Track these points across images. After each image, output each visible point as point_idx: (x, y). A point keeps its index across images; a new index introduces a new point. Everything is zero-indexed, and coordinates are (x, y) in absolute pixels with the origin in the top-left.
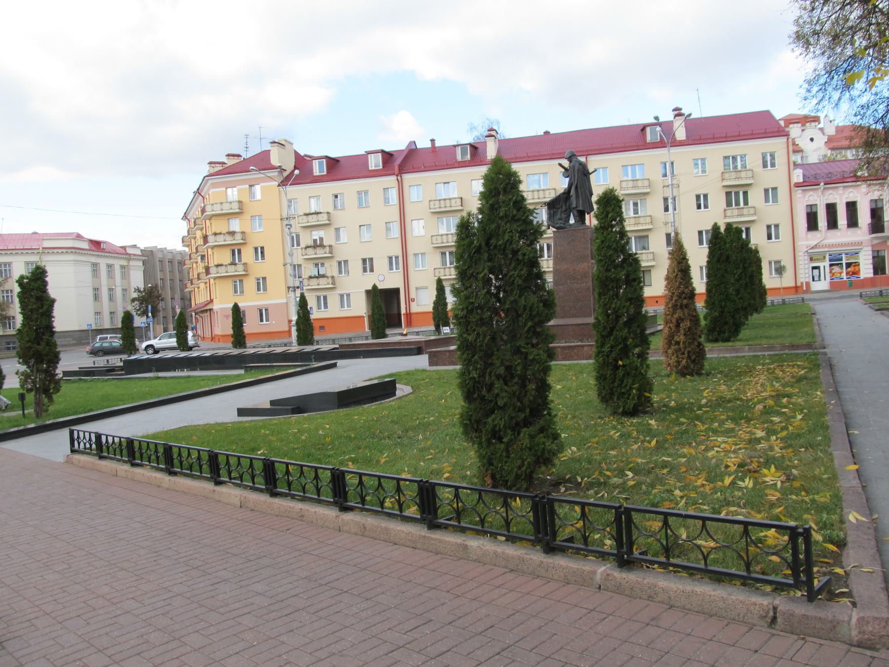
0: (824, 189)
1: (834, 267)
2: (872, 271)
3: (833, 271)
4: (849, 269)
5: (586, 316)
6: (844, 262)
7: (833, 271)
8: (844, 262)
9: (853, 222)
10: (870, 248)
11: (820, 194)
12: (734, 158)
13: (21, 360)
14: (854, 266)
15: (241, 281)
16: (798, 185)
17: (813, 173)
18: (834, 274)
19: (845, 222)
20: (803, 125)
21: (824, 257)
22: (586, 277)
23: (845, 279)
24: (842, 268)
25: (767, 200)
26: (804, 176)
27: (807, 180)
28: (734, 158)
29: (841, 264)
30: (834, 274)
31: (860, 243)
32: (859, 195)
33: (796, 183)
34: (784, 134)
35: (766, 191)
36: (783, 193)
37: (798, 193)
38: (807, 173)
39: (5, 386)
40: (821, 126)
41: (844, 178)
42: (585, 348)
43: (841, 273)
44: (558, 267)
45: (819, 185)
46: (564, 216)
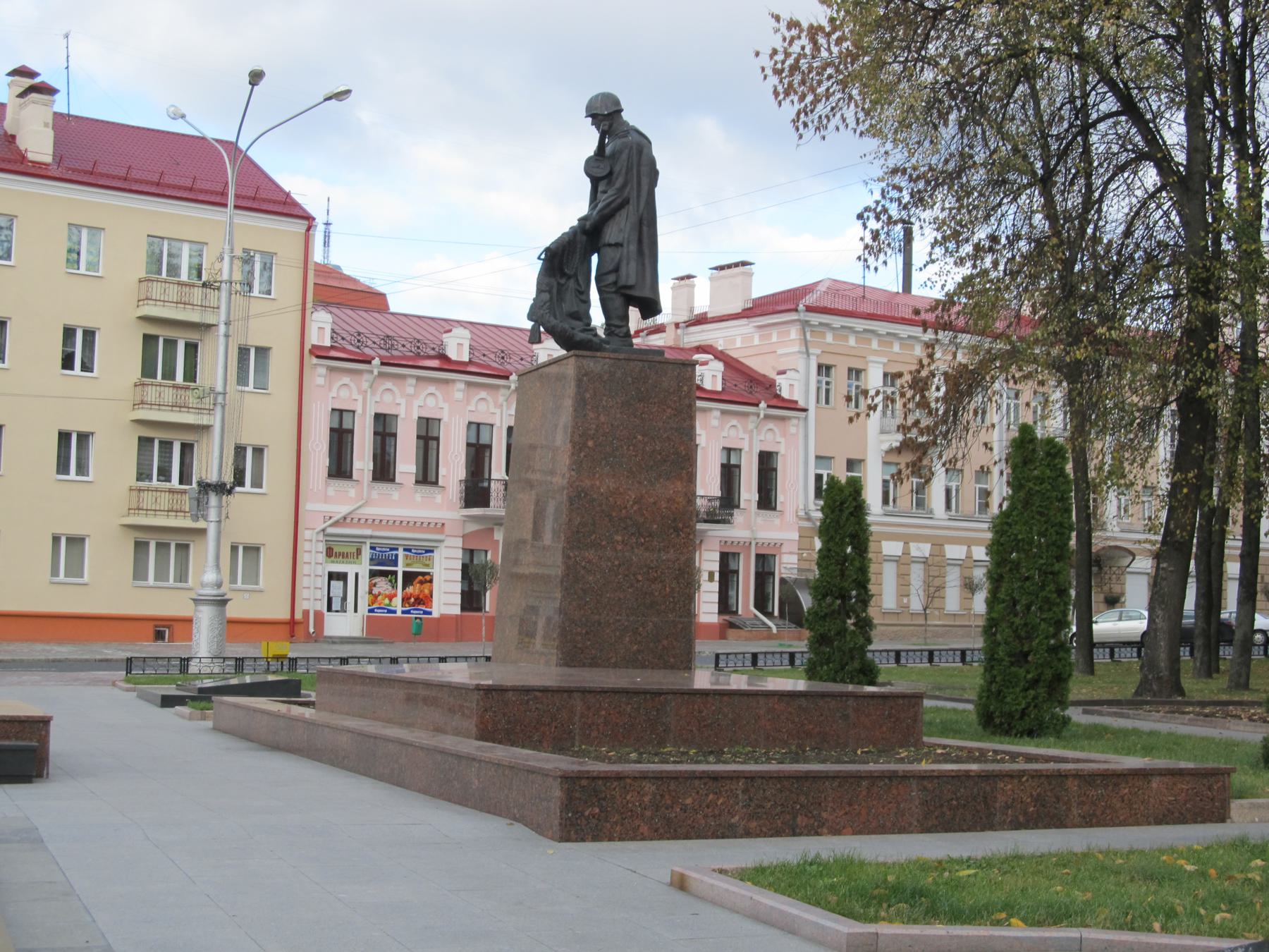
1: (377, 580)
2: (458, 599)
3: (376, 591)
4: (410, 590)
5: (672, 667)
6: (400, 569)
7: (376, 591)
8: (400, 569)
9: (427, 476)
10: (459, 542)
11: (365, 385)
14: (421, 583)
15: (182, 548)
16: (320, 353)
18: (376, 597)
21: (359, 552)
22: (676, 530)
23: (399, 614)
24: (394, 586)
29: (395, 573)
30: (376, 597)
31: (440, 527)
32: (446, 406)
33: (314, 347)
36: (282, 364)
37: (318, 373)
39: (631, 308)
41: (418, 356)
43: (391, 597)
44: (587, 483)
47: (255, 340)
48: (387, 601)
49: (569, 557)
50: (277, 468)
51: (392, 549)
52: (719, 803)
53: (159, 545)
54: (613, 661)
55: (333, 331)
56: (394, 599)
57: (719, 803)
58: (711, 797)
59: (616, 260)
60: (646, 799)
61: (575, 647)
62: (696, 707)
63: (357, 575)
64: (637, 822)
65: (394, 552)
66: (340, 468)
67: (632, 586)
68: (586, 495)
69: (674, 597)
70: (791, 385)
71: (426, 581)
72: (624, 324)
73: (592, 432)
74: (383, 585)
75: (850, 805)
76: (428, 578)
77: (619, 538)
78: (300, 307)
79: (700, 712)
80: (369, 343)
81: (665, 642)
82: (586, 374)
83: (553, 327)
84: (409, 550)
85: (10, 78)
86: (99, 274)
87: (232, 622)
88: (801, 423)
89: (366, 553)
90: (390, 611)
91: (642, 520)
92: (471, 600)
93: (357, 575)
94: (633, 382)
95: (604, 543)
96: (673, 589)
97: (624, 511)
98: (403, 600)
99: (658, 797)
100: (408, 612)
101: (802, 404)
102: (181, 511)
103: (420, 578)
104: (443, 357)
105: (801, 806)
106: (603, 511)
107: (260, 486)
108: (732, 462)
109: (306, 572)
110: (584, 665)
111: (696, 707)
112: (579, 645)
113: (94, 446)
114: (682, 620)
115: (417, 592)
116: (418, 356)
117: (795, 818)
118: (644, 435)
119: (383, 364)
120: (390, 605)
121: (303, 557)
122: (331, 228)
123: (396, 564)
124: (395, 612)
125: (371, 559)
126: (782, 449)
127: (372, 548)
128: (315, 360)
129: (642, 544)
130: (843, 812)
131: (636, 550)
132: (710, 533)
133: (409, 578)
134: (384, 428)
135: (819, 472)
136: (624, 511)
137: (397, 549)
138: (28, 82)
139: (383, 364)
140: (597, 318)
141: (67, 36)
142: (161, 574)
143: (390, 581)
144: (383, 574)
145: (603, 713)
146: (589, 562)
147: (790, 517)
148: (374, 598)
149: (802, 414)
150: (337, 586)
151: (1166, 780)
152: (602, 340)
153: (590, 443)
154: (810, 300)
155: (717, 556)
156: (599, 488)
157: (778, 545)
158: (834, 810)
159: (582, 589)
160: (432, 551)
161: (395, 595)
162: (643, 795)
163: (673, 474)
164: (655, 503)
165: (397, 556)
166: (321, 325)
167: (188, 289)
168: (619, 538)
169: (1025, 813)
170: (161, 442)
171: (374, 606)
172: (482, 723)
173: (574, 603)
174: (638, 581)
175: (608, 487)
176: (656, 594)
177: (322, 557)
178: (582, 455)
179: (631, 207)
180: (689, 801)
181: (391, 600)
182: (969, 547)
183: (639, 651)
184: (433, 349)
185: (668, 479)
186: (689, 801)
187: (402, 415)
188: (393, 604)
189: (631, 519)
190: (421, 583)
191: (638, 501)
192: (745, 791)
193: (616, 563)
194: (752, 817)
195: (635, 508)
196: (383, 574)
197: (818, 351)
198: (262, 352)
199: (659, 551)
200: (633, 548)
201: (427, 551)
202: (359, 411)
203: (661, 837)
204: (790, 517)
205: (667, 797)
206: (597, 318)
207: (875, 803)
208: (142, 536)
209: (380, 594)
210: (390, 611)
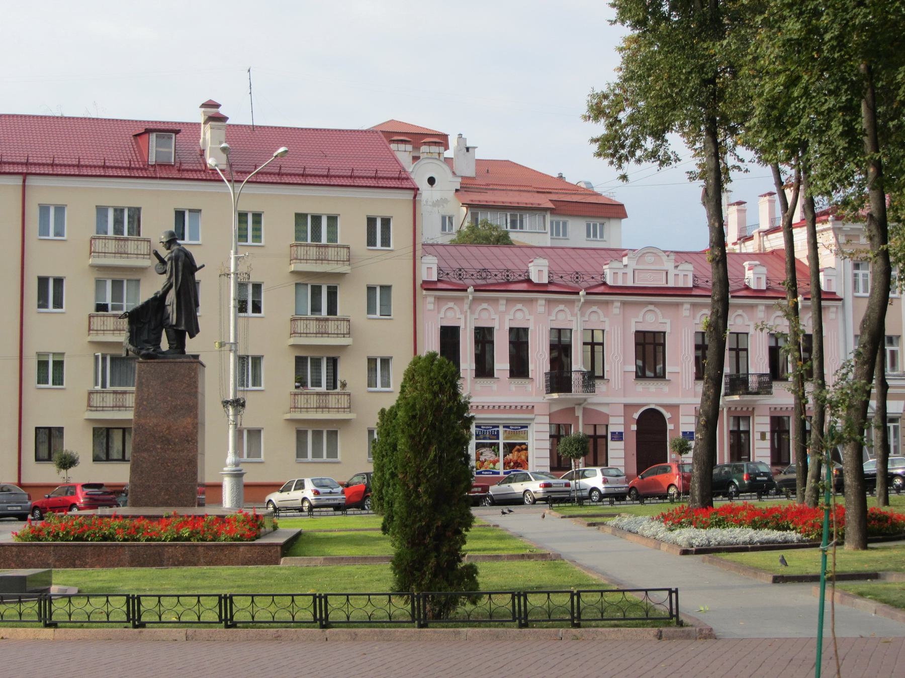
0: (474, 299)
1: (483, 450)
2: (547, 462)
3: (482, 458)
4: (510, 457)
5: (186, 506)
6: (501, 441)
7: (482, 458)
8: (501, 441)
9: (519, 368)
10: (546, 419)
11: (466, 307)
12: (317, 219)
14: (519, 451)
15: (333, 434)
16: (428, 286)
17: (456, 266)
18: (483, 463)
19: (507, 366)
20: (416, 148)
22: (188, 441)
23: (502, 474)
25: (371, 309)
26: (440, 269)
27: (445, 278)
28: (317, 219)
29: (498, 444)
30: (483, 463)
31: (530, 409)
32: (531, 318)
33: (425, 282)
34: (406, 184)
35: (371, 289)
36: (401, 299)
37: (428, 301)
38: (443, 265)
40: (448, 154)
41: (509, 282)
42: (241, 549)
43: (495, 463)
44: (143, 421)
45: (466, 290)
46: (153, 337)
47: (377, 281)
48: (491, 466)
49: (134, 456)
51: (522, 427)
53: (314, 432)
56: (497, 464)
60: (14, 554)
64: (10, 562)
65: (496, 429)
67: (165, 468)
70: (829, 280)
71: (522, 450)
76: (524, 447)
77: (159, 446)
78: (412, 254)
81: (182, 494)
84: (508, 427)
85: (203, 109)
86: (263, 243)
87: (247, 486)
88: (840, 310)
90: (494, 473)
92: (779, 456)
96: (186, 470)
98: (504, 464)
101: (840, 294)
102: (326, 408)
104: (528, 281)
107: (388, 385)
108: (779, 345)
113: (264, 364)
115: (515, 458)
116: (509, 282)
117: (74, 561)
118: (171, 397)
119: (476, 291)
120: (494, 468)
123: (498, 438)
124: (498, 473)
127: (477, 427)
128: (424, 292)
132: (759, 403)
133: (510, 447)
134: (484, 337)
137: (498, 427)
138: (212, 111)
139: (476, 291)
141: (249, 71)
142: (317, 453)
143: (494, 450)
146: (144, 458)
149: (839, 303)
151: (247, 548)
155: (767, 420)
160: (527, 427)
161: (498, 461)
165: (498, 431)
166: (429, 266)
167: (323, 249)
169: (178, 561)
170: (311, 359)
171: (482, 470)
180: (31, 554)
181: (494, 465)
184: (520, 275)
186: (31, 554)
187: (497, 327)
188: (496, 467)
190: (519, 451)
191: (169, 428)
192: (53, 551)
194: (57, 561)
198: (386, 289)
201: (522, 427)
203: (20, 568)
208: (302, 427)
209: (485, 460)
210: (494, 473)
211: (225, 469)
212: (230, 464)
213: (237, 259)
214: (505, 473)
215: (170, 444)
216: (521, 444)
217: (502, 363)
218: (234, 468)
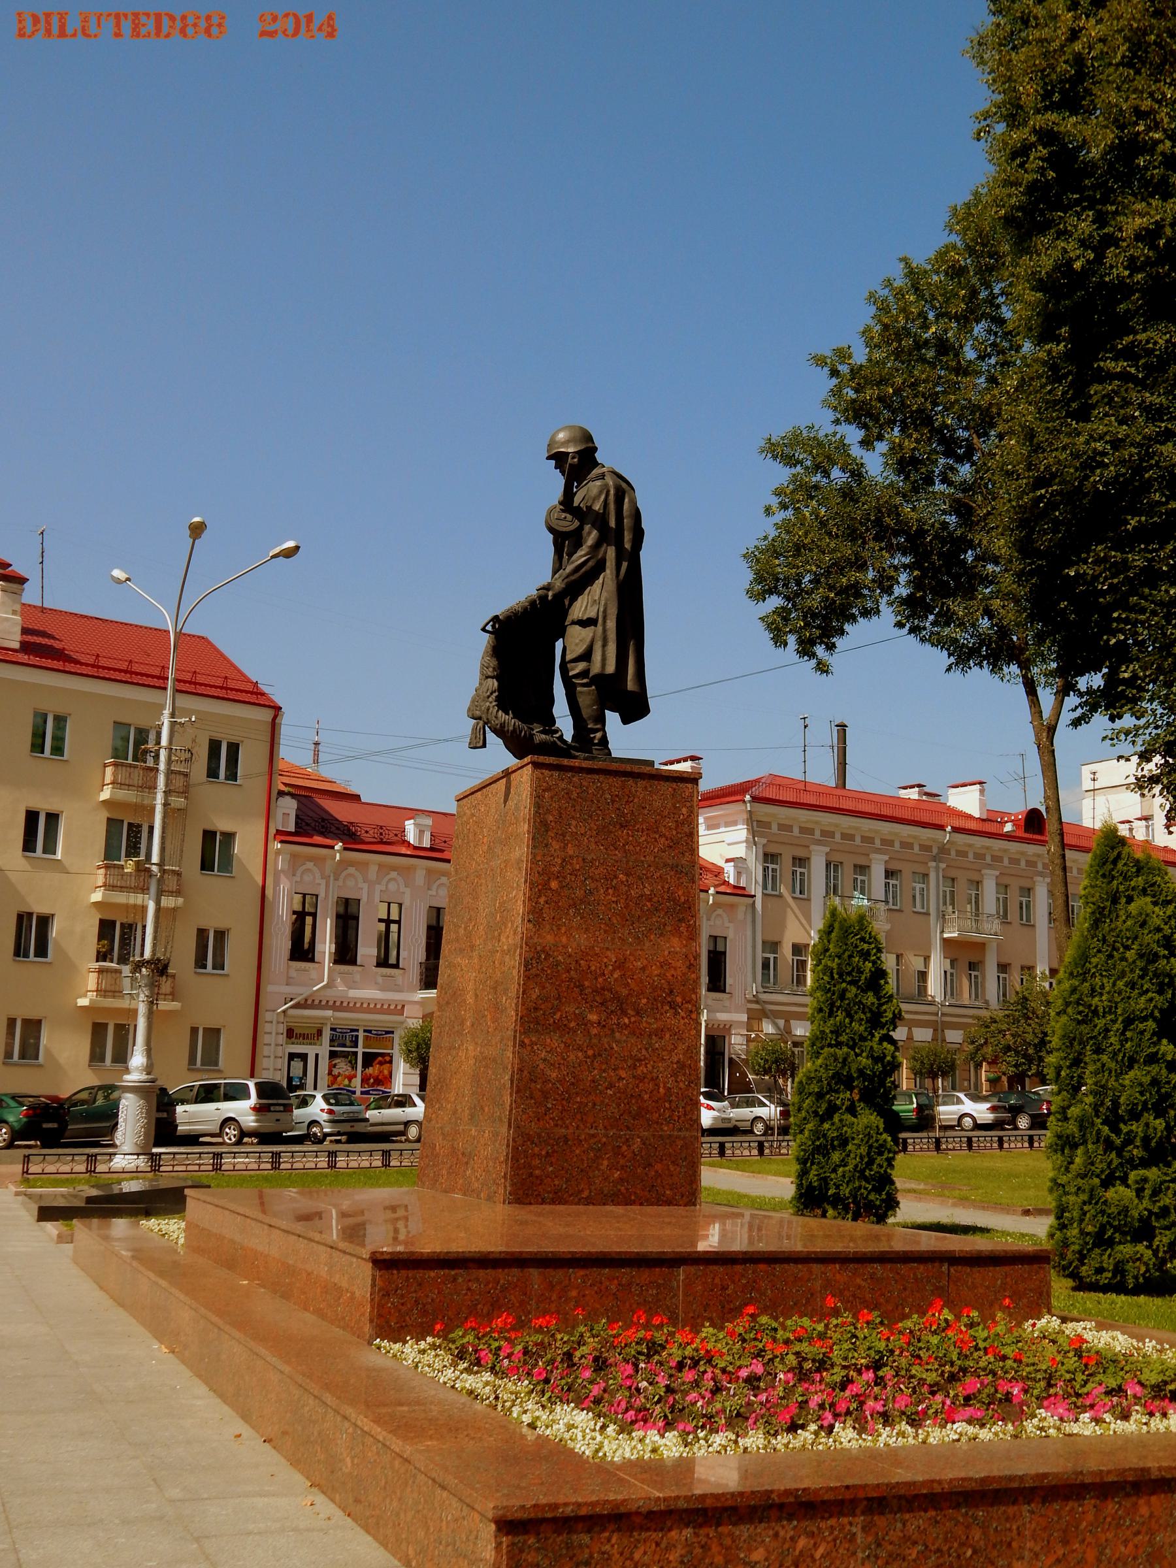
1: (337, 1061)
3: (335, 1072)
4: (370, 1070)
5: (669, 1203)
6: (360, 1050)
7: (335, 1072)
8: (360, 1050)
13: (882, 982)
14: (381, 1063)
18: (335, 1077)
21: (320, 1033)
22: (673, 1006)
23: (358, 1094)
24: (354, 1067)
29: (355, 1054)
32: (408, 891)
39: (607, 712)
43: (350, 1078)
44: (550, 938)
48: (346, 1082)
50: (239, 952)
51: (387, 1032)
52: (818, 1555)
54: (585, 1194)
55: (297, 816)
57: (818, 1555)
58: (802, 1542)
59: (588, 640)
61: (531, 1175)
62: (717, 1281)
63: (317, 1055)
66: (302, 951)
68: (548, 955)
69: (670, 1102)
71: (386, 1062)
72: (599, 726)
73: (557, 869)
74: (342, 1067)
75: (1065, 1542)
76: (387, 1058)
77: (593, 1017)
79: (724, 1288)
80: (333, 829)
81: (658, 1167)
82: (548, 789)
83: (503, 725)
86: (65, 758)
89: (327, 1034)
91: (625, 992)
93: (317, 1055)
94: (613, 801)
95: (572, 1024)
97: (600, 980)
99: (698, 1551)
100: (367, 1093)
103: (380, 1058)
105: (975, 1552)
106: (571, 979)
109: (266, 1053)
110: (543, 1202)
111: (717, 1281)
112: (537, 1172)
114: (682, 1134)
118: (627, 875)
121: (264, 1039)
122: (320, 747)
124: (354, 1092)
125: (332, 1040)
126: (730, 935)
127: (332, 1029)
129: (627, 1026)
130: (1052, 1559)
131: (617, 1035)
135: (768, 955)
136: (600, 980)
137: (357, 1030)
140: (565, 725)
143: (350, 1062)
144: (345, 1055)
145: (574, 1293)
147: (738, 998)
148: (334, 1078)
150: (297, 1065)
152: (569, 746)
153: (554, 885)
154: (755, 791)
156: (565, 947)
157: (727, 1028)
158: (1037, 1555)
159: (541, 1090)
160: (392, 1032)
161: (355, 1076)
162: (668, 1549)
163: (669, 928)
164: (643, 969)
165: (357, 1037)
166: (286, 811)
168: (593, 1017)
172: (380, 1316)
173: (529, 1111)
174: (621, 1079)
175: (579, 945)
176: (646, 1097)
177: (282, 1039)
178: (542, 900)
179: (608, 571)
181: (350, 1081)
182: (910, 1029)
183: (621, 1179)
185: (661, 935)
189: (610, 990)
191: (620, 965)
193: (590, 1053)
195: (616, 976)
196: (345, 1055)
197: (764, 841)
199: (650, 1036)
200: (613, 1031)
202: (322, 896)
204: (738, 998)
205: (715, 1549)
206: (565, 725)
207: (1110, 1535)
211: (127, 1077)
212: (137, 1068)
213: (173, 725)
214: (362, 1093)
215: (624, 1013)
216: (382, 1055)
217: (367, 950)
218: (144, 1077)
